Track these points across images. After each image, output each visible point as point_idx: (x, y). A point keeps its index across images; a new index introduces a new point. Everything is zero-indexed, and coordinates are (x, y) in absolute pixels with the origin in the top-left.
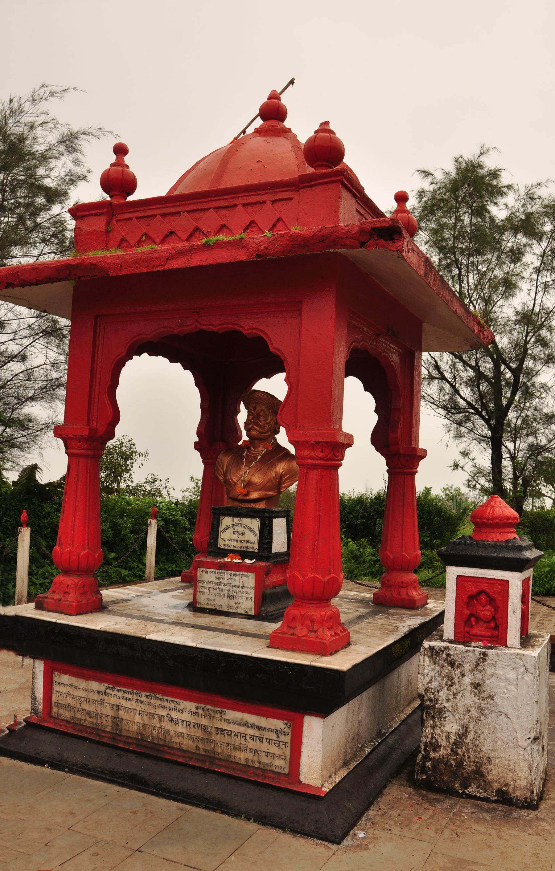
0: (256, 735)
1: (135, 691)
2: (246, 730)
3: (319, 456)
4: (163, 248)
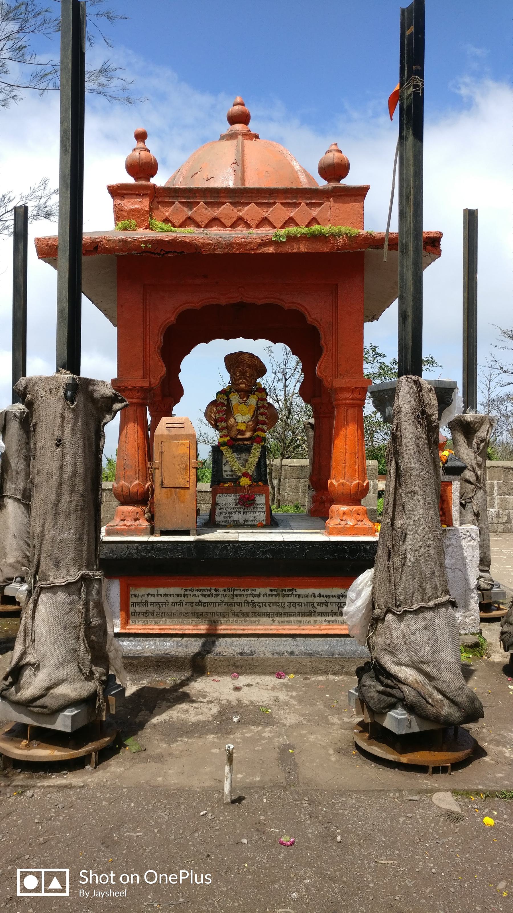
0: (322, 602)
1: (213, 588)
2: (313, 600)
3: (358, 397)
4: (283, 232)
